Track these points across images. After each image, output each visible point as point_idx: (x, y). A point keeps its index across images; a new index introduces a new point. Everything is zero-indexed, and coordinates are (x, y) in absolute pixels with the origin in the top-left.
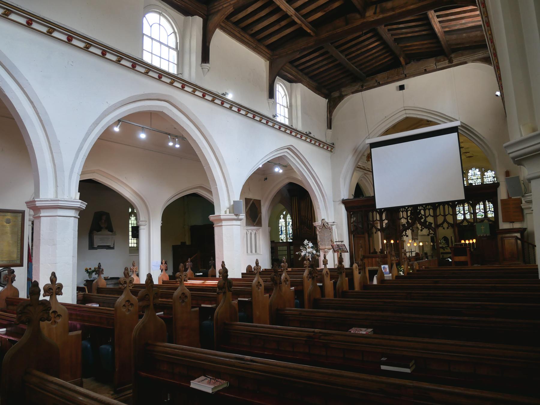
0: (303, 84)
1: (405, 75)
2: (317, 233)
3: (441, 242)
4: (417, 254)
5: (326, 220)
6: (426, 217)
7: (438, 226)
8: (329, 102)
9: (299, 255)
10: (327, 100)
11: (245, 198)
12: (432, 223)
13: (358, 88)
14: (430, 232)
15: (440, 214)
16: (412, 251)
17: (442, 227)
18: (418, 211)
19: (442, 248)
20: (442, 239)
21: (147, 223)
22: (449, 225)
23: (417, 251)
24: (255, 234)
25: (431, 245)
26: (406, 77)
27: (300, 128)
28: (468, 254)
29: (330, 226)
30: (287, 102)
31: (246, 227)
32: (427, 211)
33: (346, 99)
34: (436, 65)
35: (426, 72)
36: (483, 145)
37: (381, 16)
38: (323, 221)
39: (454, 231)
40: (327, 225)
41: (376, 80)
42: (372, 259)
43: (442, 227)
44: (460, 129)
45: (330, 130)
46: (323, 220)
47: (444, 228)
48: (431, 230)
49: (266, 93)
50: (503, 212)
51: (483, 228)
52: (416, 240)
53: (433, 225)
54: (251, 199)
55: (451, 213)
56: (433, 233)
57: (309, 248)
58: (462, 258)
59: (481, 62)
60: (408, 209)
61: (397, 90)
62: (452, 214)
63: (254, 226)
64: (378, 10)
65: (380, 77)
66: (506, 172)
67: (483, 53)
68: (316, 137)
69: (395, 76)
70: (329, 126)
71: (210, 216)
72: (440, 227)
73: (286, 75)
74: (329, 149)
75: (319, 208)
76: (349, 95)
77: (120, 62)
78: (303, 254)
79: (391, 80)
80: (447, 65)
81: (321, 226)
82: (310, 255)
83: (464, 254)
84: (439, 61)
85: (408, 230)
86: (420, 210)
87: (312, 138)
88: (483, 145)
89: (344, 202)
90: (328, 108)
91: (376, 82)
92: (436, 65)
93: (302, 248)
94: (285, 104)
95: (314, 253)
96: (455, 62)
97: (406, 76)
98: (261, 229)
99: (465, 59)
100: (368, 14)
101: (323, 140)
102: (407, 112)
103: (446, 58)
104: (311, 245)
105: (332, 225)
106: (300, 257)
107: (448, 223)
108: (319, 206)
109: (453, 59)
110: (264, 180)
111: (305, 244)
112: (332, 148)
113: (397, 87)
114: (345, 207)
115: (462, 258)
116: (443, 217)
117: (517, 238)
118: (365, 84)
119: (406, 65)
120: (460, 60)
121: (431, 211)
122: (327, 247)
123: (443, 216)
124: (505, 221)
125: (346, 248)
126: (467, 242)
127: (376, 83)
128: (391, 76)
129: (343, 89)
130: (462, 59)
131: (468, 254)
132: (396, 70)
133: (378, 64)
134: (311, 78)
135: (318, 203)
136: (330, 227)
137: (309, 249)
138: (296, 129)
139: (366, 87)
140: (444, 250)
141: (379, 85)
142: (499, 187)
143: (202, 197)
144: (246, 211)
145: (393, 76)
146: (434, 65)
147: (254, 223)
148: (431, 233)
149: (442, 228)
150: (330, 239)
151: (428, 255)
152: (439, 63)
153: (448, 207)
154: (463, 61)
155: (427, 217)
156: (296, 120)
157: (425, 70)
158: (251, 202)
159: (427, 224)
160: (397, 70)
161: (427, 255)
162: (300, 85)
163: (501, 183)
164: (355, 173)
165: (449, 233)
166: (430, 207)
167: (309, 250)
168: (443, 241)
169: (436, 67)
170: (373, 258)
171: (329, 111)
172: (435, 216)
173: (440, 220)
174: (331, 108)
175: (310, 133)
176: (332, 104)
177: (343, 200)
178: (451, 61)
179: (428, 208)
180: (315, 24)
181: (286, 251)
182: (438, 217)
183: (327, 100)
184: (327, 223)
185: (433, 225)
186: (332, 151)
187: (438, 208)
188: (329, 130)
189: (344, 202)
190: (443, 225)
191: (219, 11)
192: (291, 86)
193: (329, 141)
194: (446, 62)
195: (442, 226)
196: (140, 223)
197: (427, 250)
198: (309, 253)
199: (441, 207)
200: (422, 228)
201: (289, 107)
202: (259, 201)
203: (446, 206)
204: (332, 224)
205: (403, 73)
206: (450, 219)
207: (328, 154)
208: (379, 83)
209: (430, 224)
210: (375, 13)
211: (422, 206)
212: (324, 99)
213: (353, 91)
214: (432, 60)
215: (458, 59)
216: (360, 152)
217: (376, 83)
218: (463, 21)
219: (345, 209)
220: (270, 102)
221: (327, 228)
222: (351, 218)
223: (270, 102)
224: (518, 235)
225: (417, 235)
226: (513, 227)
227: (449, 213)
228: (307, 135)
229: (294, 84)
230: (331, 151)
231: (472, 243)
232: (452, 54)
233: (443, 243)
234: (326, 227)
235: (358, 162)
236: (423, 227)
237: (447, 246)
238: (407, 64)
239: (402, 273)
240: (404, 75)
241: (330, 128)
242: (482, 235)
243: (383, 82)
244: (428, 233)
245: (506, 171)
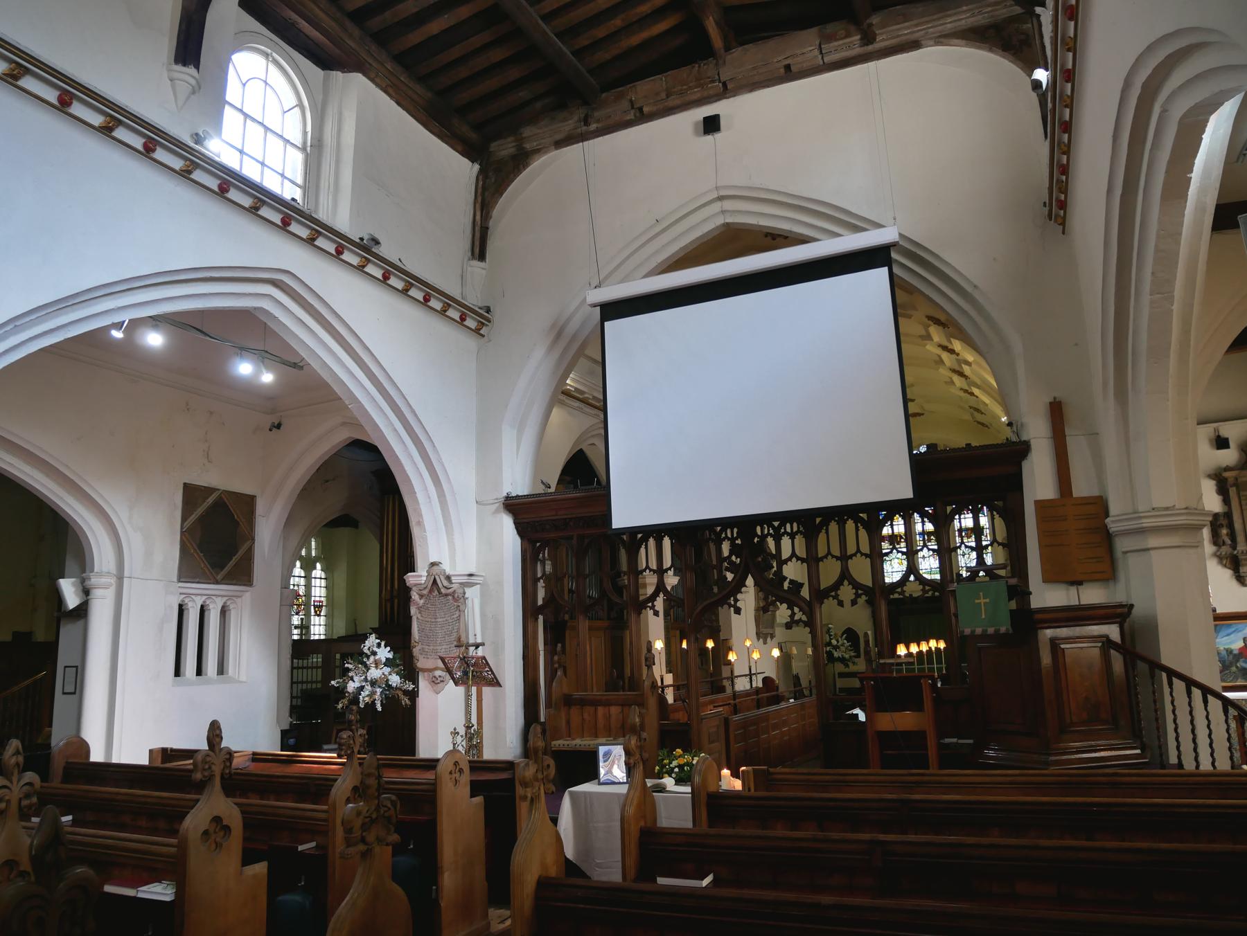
0: (372, 80)
1: (725, 84)
2: (413, 610)
3: (840, 643)
4: (767, 680)
5: (447, 567)
6: (782, 563)
7: (820, 595)
8: (483, 172)
9: (341, 692)
10: (477, 167)
11: (185, 484)
12: (802, 585)
13: (576, 129)
14: (793, 614)
15: (829, 553)
16: (748, 673)
17: (836, 597)
18: (756, 540)
19: (842, 660)
20: (842, 635)
21: (113, 581)
22: (860, 592)
23: (771, 673)
24: (224, 611)
25: (808, 656)
26: (726, 91)
27: (343, 221)
28: (928, 703)
29: (455, 586)
30: (305, 133)
31: (181, 584)
32: (786, 542)
33: (537, 164)
34: (821, 51)
35: (789, 74)
36: (973, 313)
38: (435, 569)
39: (875, 616)
40: (446, 583)
41: (631, 101)
42: (596, 710)
43: (836, 597)
44: (896, 261)
45: (482, 264)
46: (433, 564)
47: (841, 604)
48: (796, 609)
49: (166, 44)
50: (1042, 547)
51: (982, 601)
52: (769, 639)
53: (805, 592)
54: (209, 490)
55: (865, 548)
56: (804, 618)
57: (377, 663)
58: (905, 720)
59: (964, 42)
60: (723, 535)
62: (655, 568)
63: (217, 583)
66: (1050, 403)
67: (969, 10)
68: (410, 267)
69: (690, 88)
70: (477, 250)
71: (409, 574)
72: (827, 598)
73: (293, 25)
74: (471, 323)
75: (420, 523)
76: (546, 153)
77: (17, 81)
78: (351, 686)
79: (678, 102)
80: (857, 50)
81: (425, 588)
82: (379, 690)
85: (722, 607)
86: (763, 537)
87: (390, 269)
88: (973, 313)
89: (513, 505)
90: (480, 191)
91: (633, 108)
92: (821, 53)
93: (350, 666)
94: (297, 138)
95: (394, 685)
96: (883, 40)
97: (727, 87)
98: (248, 594)
99: (914, 32)
101: (454, 290)
102: (728, 205)
103: (852, 28)
104: (384, 653)
105: (463, 585)
106: (344, 697)
107: (856, 585)
108: (421, 515)
109: (877, 32)
110: (270, 430)
111: (366, 650)
112: (483, 324)
113: (696, 124)
114: (515, 523)
115: (905, 720)
116: (839, 562)
117: (1107, 643)
118: (597, 114)
119: (726, 51)
120: (898, 36)
121: (800, 541)
123: (837, 558)
124: (1052, 576)
125: (491, 670)
126: (914, 649)
127: (632, 112)
128: (680, 88)
129: (527, 132)
130: (905, 31)
131: (928, 703)
132: (694, 67)
133: (635, 40)
134: (400, 59)
135: (418, 504)
136: (455, 591)
137: (377, 667)
138: (308, 212)
139: (599, 125)
140: (847, 666)
141: (643, 117)
142: (1029, 457)
144: (182, 528)
145: (685, 87)
146: (816, 52)
147: (218, 574)
148: (796, 618)
150: (455, 635)
151: (803, 686)
152: (832, 45)
153: (857, 530)
154: (908, 37)
155: (786, 561)
156: (330, 197)
157: (788, 67)
158: (211, 500)
159: (786, 585)
160: (697, 69)
161: (801, 685)
162: (359, 78)
163: (1034, 445)
164: (556, 412)
165: (859, 618)
166: (795, 529)
167: (374, 673)
168: (845, 641)
169: (820, 57)
170: (611, 705)
171: (479, 199)
172: (812, 560)
173: (829, 572)
174: (486, 194)
175: (377, 242)
176: (493, 180)
177: (508, 498)
178: (868, 38)
179: (789, 530)
181: (320, 670)
182: (821, 563)
184: (448, 578)
185: (805, 592)
186: (482, 332)
187: (824, 531)
188: (476, 263)
189: (513, 505)
190: (839, 592)
192: (326, 80)
193: (474, 299)
194: (853, 44)
195: (833, 594)
196: (92, 580)
197: (801, 667)
198: (374, 683)
199: (833, 527)
200: (767, 602)
201: (309, 149)
202: (249, 502)
203: (850, 525)
204: (464, 580)
205: (717, 77)
206: (860, 569)
207: (470, 342)
208: (641, 109)
209: (796, 586)
211: (770, 525)
212: (465, 161)
213: (558, 137)
214: (811, 35)
215: (893, 31)
216: (574, 337)
217: (632, 112)
219: (516, 532)
220: (176, 75)
221: (447, 595)
222: (535, 559)
223: (176, 75)
224: (1113, 631)
225: (772, 624)
226: (1079, 602)
227: (858, 550)
228: (367, 248)
229: (337, 75)
230: (477, 331)
231: (927, 651)
232: (874, 16)
233: (843, 648)
234: (443, 591)
235: (565, 376)
236: (771, 598)
237: (855, 654)
238: (728, 49)
239: (673, 781)
240: (721, 85)
241: (482, 257)
242: (979, 631)
243: (654, 109)
244: (789, 620)
245: (1052, 400)
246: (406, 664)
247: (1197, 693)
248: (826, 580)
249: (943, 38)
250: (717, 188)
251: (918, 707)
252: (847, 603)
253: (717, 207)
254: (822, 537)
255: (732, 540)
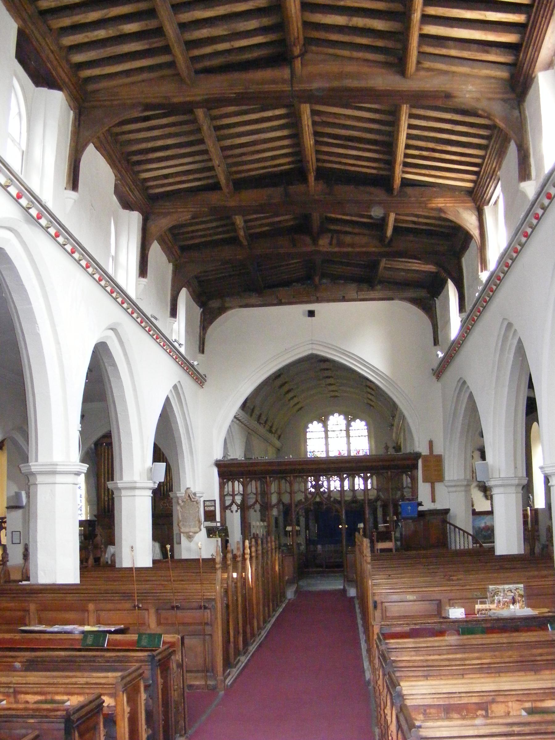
1: (317, 298)
5: (193, 490)
8: (203, 313)
26: (318, 300)
29: (197, 498)
33: (230, 313)
37: (336, 249)
43: (230, 509)
45: (202, 355)
46: (188, 489)
47: (232, 512)
61: (304, 315)
64: (335, 241)
65: (282, 292)
70: (201, 349)
83: (526, 510)
84: (361, 290)
100: (321, 242)
107: (236, 504)
122: (193, 530)
129: (228, 299)
141: (280, 303)
143: (28, 444)
149: (253, 510)
150: (197, 518)
180: (253, 237)
183: (202, 309)
184: (195, 494)
191: (169, 213)
208: (281, 300)
210: (331, 244)
212: (199, 308)
213: (241, 304)
214: (354, 286)
218: (410, 264)
227: (239, 492)
234: (193, 500)
246: (190, 532)
247: (461, 532)
248: (228, 503)
249: (402, 299)
250: (312, 340)
251: (391, 540)
252: (234, 511)
253: (310, 346)
254: (249, 487)
255: (311, 482)
